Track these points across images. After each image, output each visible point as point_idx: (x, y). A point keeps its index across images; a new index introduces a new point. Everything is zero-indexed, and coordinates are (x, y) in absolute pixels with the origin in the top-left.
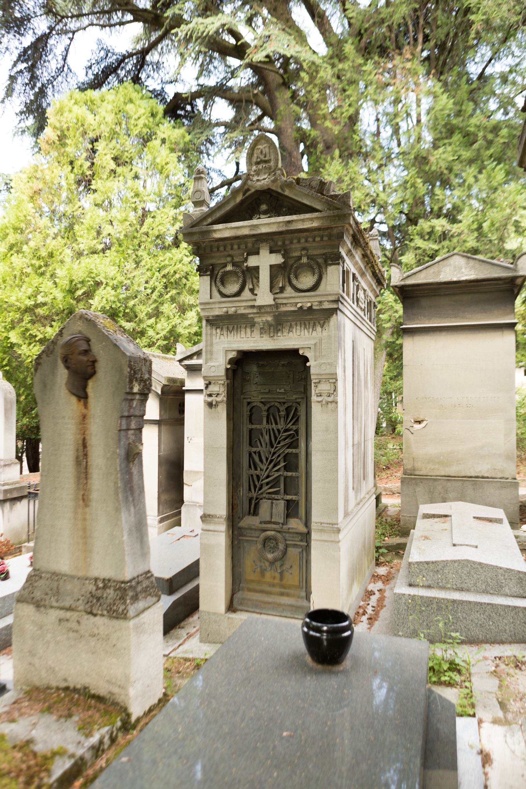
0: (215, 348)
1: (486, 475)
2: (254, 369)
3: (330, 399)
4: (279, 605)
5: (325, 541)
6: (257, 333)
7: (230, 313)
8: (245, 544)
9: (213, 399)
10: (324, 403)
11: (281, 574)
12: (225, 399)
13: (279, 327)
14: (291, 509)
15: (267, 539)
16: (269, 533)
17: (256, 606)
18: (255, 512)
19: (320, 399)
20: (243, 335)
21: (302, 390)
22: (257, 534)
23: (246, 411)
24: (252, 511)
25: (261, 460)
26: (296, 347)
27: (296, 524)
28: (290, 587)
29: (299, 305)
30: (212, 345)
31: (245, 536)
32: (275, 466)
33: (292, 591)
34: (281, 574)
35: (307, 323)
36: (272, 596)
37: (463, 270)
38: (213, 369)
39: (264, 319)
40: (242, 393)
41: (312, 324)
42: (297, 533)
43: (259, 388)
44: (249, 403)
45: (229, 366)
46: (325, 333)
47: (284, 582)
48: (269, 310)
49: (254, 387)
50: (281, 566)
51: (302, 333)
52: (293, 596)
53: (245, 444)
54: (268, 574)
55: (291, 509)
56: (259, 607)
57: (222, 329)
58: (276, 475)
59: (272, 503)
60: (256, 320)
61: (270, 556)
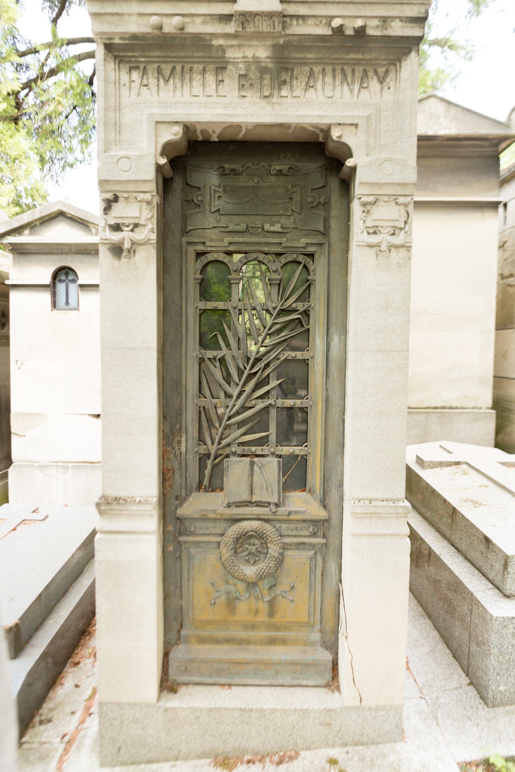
0: (128, 118)
1: (454, 405)
2: (210, 179)
3: (398, 240)
4: (268, 664)
5: (380, 535)
6: (230, 85)
7: (167, 29)
8: (193, 551)
9: (125, 236)
10: (384, 247)
11: (272, 604)
12: (154, 236)
13: (284, 76)
14: (295, 473)
15: (243, 538)
16: (247, 525)
17: (219, 673)
18: (213, 482)
19: (374, 239)
20: (197, 88)
21: (321, 228)
22: (219, 528)
23: (192, 269)
24: (206, 482)
25: (228, 378)
26: (326, 121)
27: (302, 504)
28: (287, 627)
29: (336, 22)
30: (119, 108)
31: (192, 534)
32: (258, 386)
33: (292, 634)
34: (272, 604)
35: (348, 70)
36: (251, 647)
37: (442, 120)
38: (125, 164)
39: (249, 53)
40: (185, 232)
41: (358, 74)
42: (304, 521)
43: (224, 221)
44: (199, 255)
45: (163, 161)
46: (388, 96)
47: (277, 619)
48: (264, 27)
49: (211, 220)
50: (272, 587)
51: (338, 89)
52: (295, 642)
53: (191, 342)
54: (242, 607)
55: (295, 473)
56: (224, 675)
57: (145, 72)
58: (261, 405)
59: (252, 464)
60: (230, 54)
61: (250, 571)
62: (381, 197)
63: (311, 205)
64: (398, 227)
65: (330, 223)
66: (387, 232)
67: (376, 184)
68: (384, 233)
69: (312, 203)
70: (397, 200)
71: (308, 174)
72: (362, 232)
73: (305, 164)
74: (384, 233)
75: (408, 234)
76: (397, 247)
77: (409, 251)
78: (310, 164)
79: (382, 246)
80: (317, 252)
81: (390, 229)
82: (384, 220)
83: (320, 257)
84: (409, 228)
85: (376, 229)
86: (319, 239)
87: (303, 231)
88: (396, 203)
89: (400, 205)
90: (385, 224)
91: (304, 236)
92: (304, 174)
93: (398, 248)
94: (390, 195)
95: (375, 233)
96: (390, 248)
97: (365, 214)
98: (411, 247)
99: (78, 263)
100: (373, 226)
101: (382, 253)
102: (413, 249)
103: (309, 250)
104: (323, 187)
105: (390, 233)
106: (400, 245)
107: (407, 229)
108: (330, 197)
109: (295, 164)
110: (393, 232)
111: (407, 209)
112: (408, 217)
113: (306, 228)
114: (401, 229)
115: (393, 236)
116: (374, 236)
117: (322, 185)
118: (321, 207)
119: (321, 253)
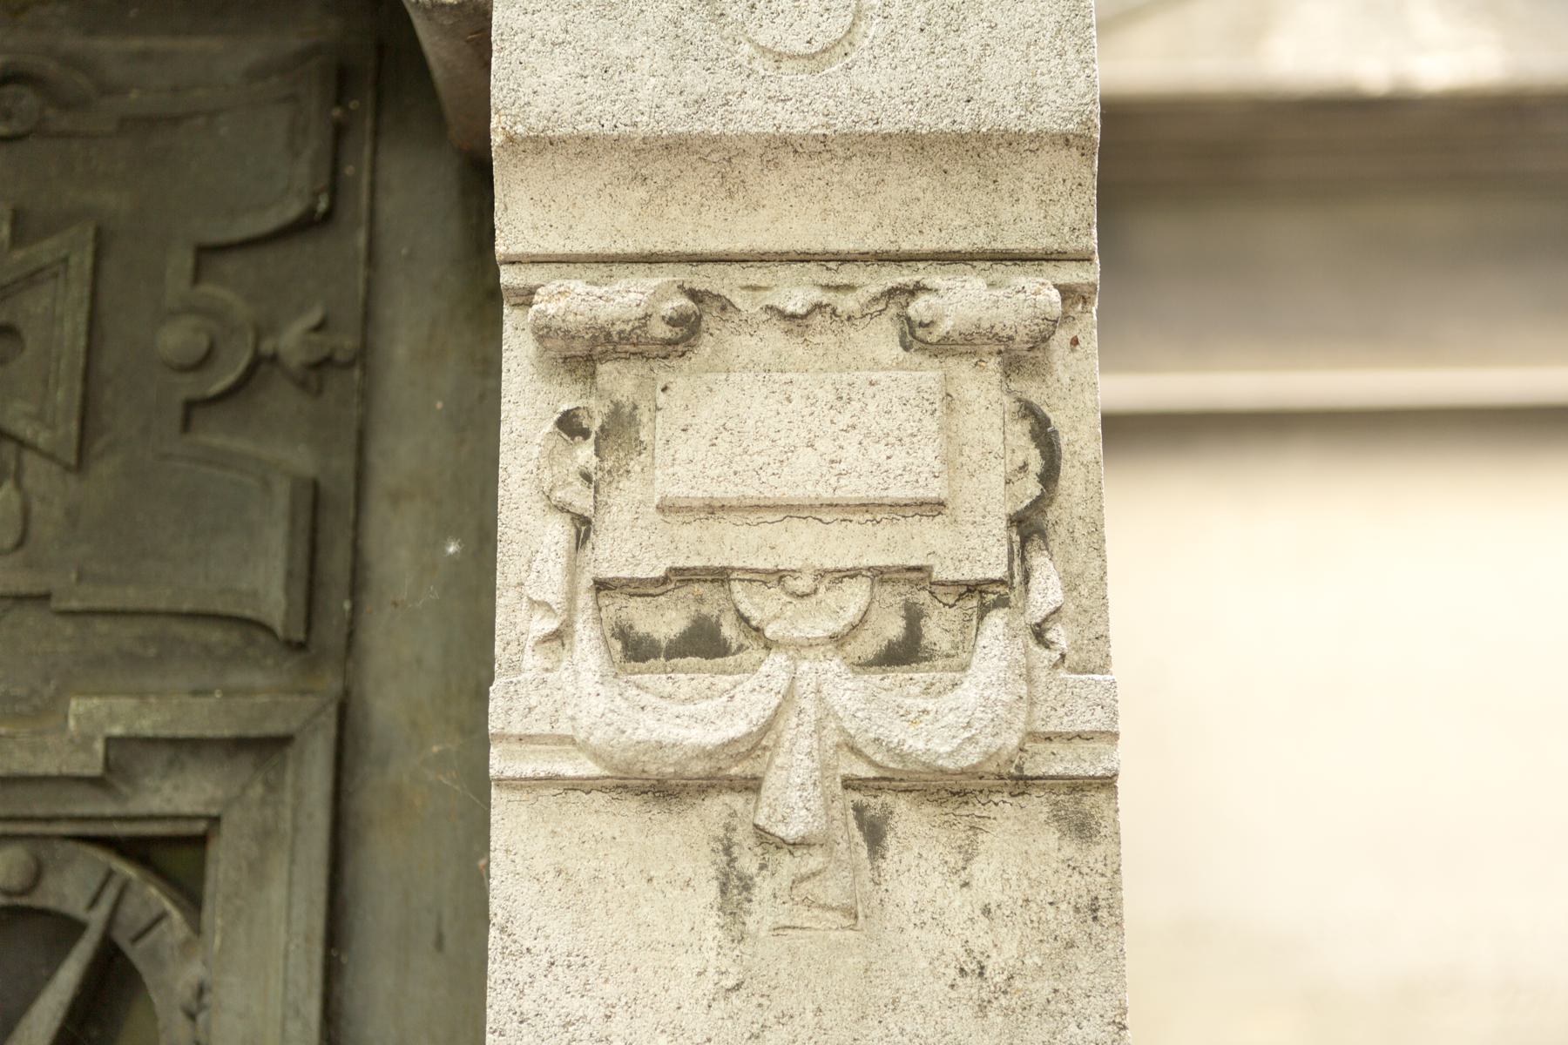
3: (957, 711)
10: (794, 796)
19: (689, 715)
21: (268, 589)
62: (756, 275)
63: (189, 386)
64: (943, 573)
65: (373, 543)
66: (824, 626)
67: (675, 146)
68: (800, 648)
69: (204, 362)
70: (919, 308)
71: (175, 120)
72: (558, 636)
73: (160, 43)
74: (800, 648)
75: (1071, 644)
76: (951, 790)
77: (1083, 829)
78: (198, 43)
79: (772, 782)
80: (234, 817)
81: (855, 596)
82: (790, 510)
83: (257, 872)
84: (1070, 587)
85: (712, 601)
86: (261, 696)
87: (102, 626)
88: (913, 336)
89: (946, 348)
90: (802, 547)
91: (97, 671)
92: (149, 123)
93: (961, 795)
94: (843, 259)
95: (703, 642)
96: (875, 803)
97: (585, 453)
98: (1107, 783)
99: (1050, 517)
100: (681, 576)
101: (788, 865)
102: (1134, 810)
103: (156, 804)
104: (308, 224)
105: (868, 645)
106: (973, 773)
107: (1047, 589)
108: (368, 316)
109: (71, 41)
110: (895, 628)
111: (1034, 392)
112: (1049, 476)
113: (132, 597)
114: (981, 595)
115: (898, 675)
116: (691, 677)
117: (293, 210)
118: (281, 399)
119: (265, 835)
